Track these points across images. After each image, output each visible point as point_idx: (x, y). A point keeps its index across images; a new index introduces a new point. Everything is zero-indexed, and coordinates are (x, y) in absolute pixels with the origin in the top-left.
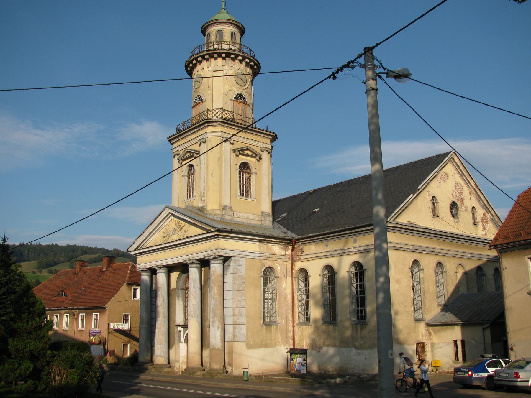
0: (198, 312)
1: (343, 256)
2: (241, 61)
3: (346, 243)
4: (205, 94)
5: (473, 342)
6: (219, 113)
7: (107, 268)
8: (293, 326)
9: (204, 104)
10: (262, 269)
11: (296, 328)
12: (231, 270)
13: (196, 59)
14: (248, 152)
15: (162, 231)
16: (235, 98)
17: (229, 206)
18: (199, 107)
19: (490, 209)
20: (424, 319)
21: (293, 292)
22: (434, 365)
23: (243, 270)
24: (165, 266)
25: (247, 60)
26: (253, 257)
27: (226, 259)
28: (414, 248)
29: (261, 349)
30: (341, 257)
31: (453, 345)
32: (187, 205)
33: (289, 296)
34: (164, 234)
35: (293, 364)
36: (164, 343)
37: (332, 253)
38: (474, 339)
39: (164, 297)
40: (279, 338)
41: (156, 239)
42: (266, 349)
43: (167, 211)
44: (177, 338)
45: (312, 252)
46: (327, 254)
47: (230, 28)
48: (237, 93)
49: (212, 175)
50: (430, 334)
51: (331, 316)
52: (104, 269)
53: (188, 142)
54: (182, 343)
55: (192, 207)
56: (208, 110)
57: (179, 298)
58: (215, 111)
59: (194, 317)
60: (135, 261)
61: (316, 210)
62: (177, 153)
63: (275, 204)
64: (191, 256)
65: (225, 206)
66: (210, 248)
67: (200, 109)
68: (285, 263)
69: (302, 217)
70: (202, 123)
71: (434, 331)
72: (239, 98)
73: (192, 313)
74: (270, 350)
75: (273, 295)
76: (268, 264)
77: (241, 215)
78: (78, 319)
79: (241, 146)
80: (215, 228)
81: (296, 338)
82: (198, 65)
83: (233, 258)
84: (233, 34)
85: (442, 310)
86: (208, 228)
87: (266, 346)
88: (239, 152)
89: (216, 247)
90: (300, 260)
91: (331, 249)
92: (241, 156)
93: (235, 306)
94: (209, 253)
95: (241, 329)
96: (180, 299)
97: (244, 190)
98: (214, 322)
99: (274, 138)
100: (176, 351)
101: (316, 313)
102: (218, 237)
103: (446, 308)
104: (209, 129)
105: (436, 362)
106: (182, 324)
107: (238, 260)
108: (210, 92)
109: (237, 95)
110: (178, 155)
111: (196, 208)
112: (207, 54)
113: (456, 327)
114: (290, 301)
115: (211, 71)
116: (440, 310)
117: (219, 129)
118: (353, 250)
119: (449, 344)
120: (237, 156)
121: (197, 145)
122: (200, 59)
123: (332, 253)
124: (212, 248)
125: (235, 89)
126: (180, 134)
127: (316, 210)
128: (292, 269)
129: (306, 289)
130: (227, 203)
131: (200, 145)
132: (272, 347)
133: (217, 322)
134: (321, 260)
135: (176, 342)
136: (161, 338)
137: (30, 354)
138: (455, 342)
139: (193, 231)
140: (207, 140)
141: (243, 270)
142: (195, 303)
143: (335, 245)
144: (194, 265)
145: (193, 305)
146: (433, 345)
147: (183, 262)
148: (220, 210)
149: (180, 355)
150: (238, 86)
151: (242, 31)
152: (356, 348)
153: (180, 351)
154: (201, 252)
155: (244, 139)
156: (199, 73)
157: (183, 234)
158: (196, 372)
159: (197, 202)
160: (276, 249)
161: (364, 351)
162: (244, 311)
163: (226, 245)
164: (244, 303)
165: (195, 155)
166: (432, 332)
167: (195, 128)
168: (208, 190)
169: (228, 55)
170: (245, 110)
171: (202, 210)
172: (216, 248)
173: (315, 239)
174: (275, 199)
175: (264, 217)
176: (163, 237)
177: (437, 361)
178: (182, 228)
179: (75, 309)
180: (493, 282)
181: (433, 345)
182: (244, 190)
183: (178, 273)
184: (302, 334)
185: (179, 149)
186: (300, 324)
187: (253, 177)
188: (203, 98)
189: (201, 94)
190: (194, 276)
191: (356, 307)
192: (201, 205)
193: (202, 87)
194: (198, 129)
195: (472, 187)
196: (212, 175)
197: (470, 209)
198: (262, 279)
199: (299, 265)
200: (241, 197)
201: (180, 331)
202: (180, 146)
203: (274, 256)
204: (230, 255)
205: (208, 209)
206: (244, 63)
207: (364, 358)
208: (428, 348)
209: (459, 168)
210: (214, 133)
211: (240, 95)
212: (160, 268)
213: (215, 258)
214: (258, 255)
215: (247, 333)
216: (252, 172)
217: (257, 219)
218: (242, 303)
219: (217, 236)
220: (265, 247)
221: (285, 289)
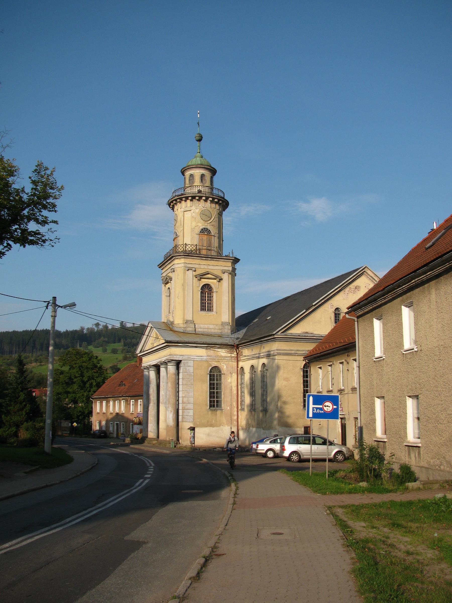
3: (260, 349)
8: (238, 412)
13: (176, 200)
23: (191, 369)
27: (178, 363)
33: (234, 389)
36: (153, 423)
40: (224, 420)
42: (211, 428)
47: (200, 171)
48: (201, 227)
49: (178, 297)
60: (141, 360)
76: (215, 364)
77: (202, 326)
78: (130, 404)
82: (175, 205)
83: (182, 361)
84: (202, 176)
87: (212, 426)
88: (201, 277)
92: (202, 280)
93: (183, 396)
95: (189, 413)
99: (236, 261)
101: (248, 400)
104: (176, 261)
109: (202, 230)
112: (178, 199)
114: (235, 392)
117: (182, 261)
122: (174, 202)
125: (200, 225)
129: (307, 377)
130: (189, 317)
132: (217, 427)
140: (175, 270)
142: (163, 394)
148: (183, 324)
151: (213, 172)
155: (203, 265)
160: (223, 352)
162: (191, 400)
169: (193, 198)
175: (223, 326)
179: (128, 397)
187: (214, 295)
196: (178, 297)
198: (209, 376)
200: (203, 313)
203: (220, 358)
206: (209, 202)
210: (179, 263)
211: (205, 229)
214: (205, 358)
217: (217, 328)
218: (190, 394)
220: (211, 352)
221: (231, 383)
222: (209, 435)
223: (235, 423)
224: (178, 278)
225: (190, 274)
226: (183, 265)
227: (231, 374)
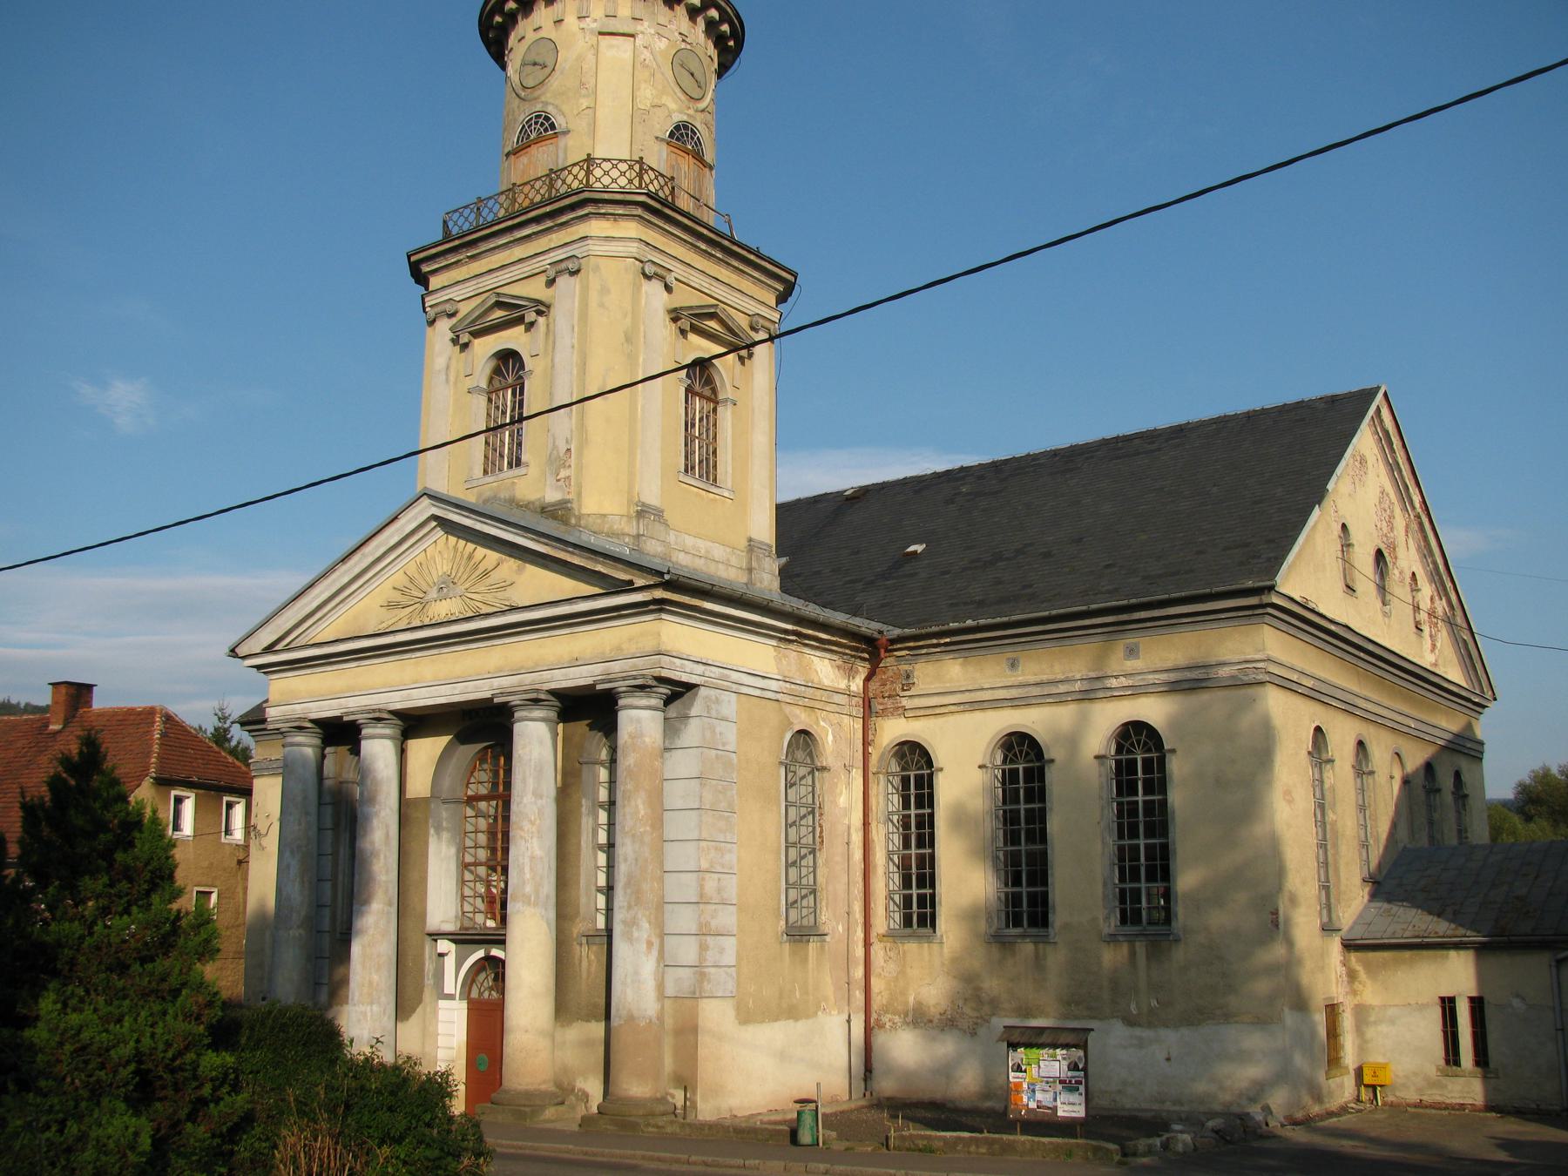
0: (549, 887)
1: (1083, 700)
2: (693, 13)
3: (1101, 659)
4: (565, 108)
5: (1516, 1002)
6: (631, 174)
7: (66, 723)
8: (867, 944)
9: (562, 141)
10: (782, 738)
11: (878, 950)
12: (692, 733)
14: (713, 324)
15: (388, 585)
16: (672, 135)
17: (656, 509)
18: (524, 159)
19: (1449, 585)
20: (1337, 926)
21: (866, 824)
22: (1367, 1080)
23: (729, 735)
24: (396, 713)
25: (714, 13)
26: (758, 693)
27: (678, 692)
28: (1319, 686)
29: (777, 1025)
30: (1086, 705)
31: (1436, 1013)
32: (488, 494)
33: (857, 838)
34: (397, 596)
35: (1019, 1085)
37: (1036, 691)
38: (1518, 996)
39: (387, 826)
41: (365, 611)
43: (426, 508)
44: (429, 981)
45: (949, 686)
46: (1014, 693)
48: (678, 117)
50: (1352, 976)
51: (1026, 903)
52: (54, 727)
53: (508, 268)
54: (451, 997)
55: (512, 502)
56: (589, 160)
57: (439, 838)
58: (615, 167)
59: (536, 904)
61: (919, 548)
62: (449, 308)
63: (786, 513)
64: (528, 678)
65: (644, 505)
66: (619, 649)
67: (540, 159)
68: (846, 719)
69: (871, 572)
70: (569, 204)
71: (1369, 968)
72: (681, 135)
73: (528, 889)
74: (801, 1026)
75: (803, 831)
76: (802, 720)
77: (690, 541)
79: (695, 300)
80: (661, 574)
81: (877, 985)
83: (703, 692)
85: (1374, 896)
86: (623, 576)
89: (649, 645)
90: (903, 712)
91: (1032, 679)
92: (692, 337)
93: (704, 865)
94: (616, 667)
95: (722, 951)
96: (445, 835)
97: (701, 461)
98: (632, 923)
100: (424, 1030)
102: (661, 610)
103: (1382, 886)
104: (596, 227)
105: (1378, 1069)
106: (450, 927)
107: (717, 701)
108: (585, 103)
109: (677, 128)
110: (451, 316)
111: (526, 506)
113: (1453, 953)
114: (858, 855)
115: (592, 32)
116: (1366, 897)
117: (631, 229)
118: (1124, 681)
119: (1422, 1007)
120: (683, 332)
121: (543, 279)
123: (1036, 691)
124: (632, 649)
125: (673, 106)
126: (461, 243)
127: (919, 548)
128: (866, 743)
131: (551, 283)
132: (808, 1017)
133: (646, 925)
134: (990, 713)
135: (428, 995)
136: (375, 977)
137: (136, 1072)
138: (1448, 1005)
139: (539, 586)
141: (729, 735)
142: (538, 853)
143: (1063, 663)
144: (538, 713)
145: (532, 858)
146: (1361, 1012)
147: (593, 686)
149: (441, 1041)
150: (683, 97)
152: (1130, 1022)
153: (441, 1028)
154: (575, 663)
156: (542, 34)
157: (489, 598)
158: (543, 1108)
159: (531, 484)
161: (1163, 1032)
162: (732, 893)
163: (686, 642)
164: (731, 858)
165: (530, 316)
166: (1359, 968)
167: (537, 220)
168: (584, 442)
170: (699, 181)
171: (558, 512)
172: (649, 648)
173: (961, 641)
174: (787, 497)
175: (758, 559)
176: (391, 606)
177: (1384, 1067)
178: (486, 574)
180: (1452, 815)
181: (1361, 1012)
182: (701, 461)
183: (443, 741)
184: (902, 972)
185: (456, 293)
186: (890, 935)
187: (725, 415)
188: (560, 122)
189: (550, 109)
190: (535, 754)
191: (1105, 873)
192: (552, 496)
193: (555, 83)
194: (549, 224)
195: (1414, 508)
197: (1408, 576)
199: (892, 730)
201: (441, 955)
202: (462, 285)
204: (694, 680)
205: (584, 511)
207: (1161, 1056)
208: (1347, 1022)
209: (1390, 444)
210: (613, 241)
212: (379, 720)
213: (642, 688)
214: (774, 685)
215: (737, 966)
216: (721, 397)
217: (734, 561)
218: (727, 857)
219: (660, 606)
222: (783, 1056)
223: (859, 996)
224: (602, 305)
225: (656, 299)
226: (633, 248)
227: (847, 769)
